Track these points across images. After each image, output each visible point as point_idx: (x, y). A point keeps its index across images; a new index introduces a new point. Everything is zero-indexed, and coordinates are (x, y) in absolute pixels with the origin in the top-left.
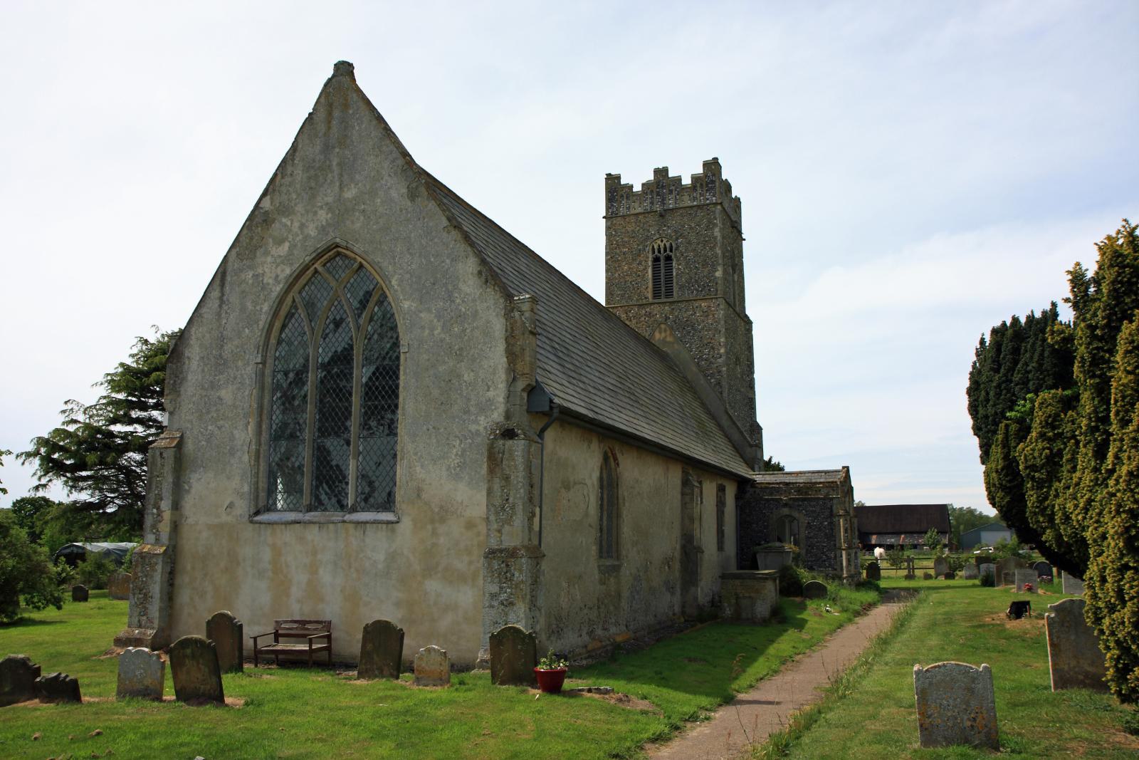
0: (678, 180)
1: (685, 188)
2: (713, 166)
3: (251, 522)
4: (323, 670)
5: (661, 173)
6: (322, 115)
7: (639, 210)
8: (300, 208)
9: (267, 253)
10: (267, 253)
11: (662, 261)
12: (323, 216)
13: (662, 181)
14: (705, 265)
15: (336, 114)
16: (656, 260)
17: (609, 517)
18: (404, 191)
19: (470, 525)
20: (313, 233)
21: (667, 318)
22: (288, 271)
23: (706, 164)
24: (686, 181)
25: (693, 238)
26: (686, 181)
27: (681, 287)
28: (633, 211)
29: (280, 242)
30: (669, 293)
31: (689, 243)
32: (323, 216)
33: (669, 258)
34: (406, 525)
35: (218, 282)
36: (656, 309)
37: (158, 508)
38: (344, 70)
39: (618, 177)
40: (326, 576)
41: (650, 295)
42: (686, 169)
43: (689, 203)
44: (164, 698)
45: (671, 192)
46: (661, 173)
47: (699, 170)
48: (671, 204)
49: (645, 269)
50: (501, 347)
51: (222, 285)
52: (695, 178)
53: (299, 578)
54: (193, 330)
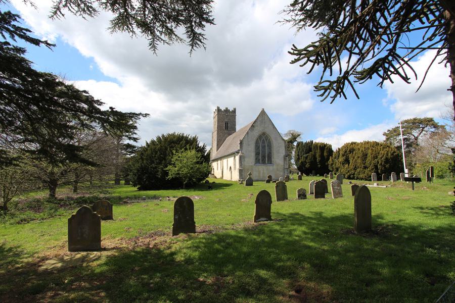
2: (235, 109)
5: (227, 108)
8: (255, 224)
13: (227, 110)
26: (231, 111)
38: (263, 109)
42: (231, 109)
46: (227, 108)
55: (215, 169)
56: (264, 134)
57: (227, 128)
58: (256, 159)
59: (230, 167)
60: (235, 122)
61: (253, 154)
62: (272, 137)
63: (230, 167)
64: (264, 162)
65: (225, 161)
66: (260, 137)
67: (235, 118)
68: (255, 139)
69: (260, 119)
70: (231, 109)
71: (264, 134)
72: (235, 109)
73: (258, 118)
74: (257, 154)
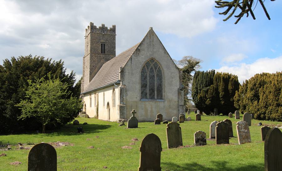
0: (107, 28)
1: (108, 30)
2: (114, 27)
3: (140, 101)
5: (103, 25)
6: (148, 36)
9: (140, 56)
10: (140, 56)
11: (103, 45)
13: (103, 28)
14: (112, 48)
16: (102, 44)
18: (163, 52)
19: (175, 102)
20: (149, 55)
21: (104, 58)
22: (144, 61)
24: (109, 28)
25: (110, 41)
27: (107, 52)
28: (96, 32)
29: (143, 55)
30: (104, 52)
31: (109, 42)
33: (104, 45)
34: (166, 102)
36: (101, 55)
37: (123, 98)
38: (152, 28)
39: (93, 24)
40: (154, 109)
41: (100, 52)
42: (109, 27)
43: (109, 34)
44: (138, 127)
45: (105, 30)
46: (103, 25)
47: (112, 27)
48: (105, 33)
49: (99, 46)
53: (149, 109)
54: (126, 67)
56: (152, 60)
57: (103, 51)
58: (142, 93)
59: (108, 104)
61: (138, 87)
62: (164, 65)
63: (108, 104)
64: (152, 97)
65: (101, 94)
66: (147, 64)
69: (147, 41)
70: (109, 27)
71: (152, 60)
72: (114, 27)
73: (144, 39)
74: (144, 86)
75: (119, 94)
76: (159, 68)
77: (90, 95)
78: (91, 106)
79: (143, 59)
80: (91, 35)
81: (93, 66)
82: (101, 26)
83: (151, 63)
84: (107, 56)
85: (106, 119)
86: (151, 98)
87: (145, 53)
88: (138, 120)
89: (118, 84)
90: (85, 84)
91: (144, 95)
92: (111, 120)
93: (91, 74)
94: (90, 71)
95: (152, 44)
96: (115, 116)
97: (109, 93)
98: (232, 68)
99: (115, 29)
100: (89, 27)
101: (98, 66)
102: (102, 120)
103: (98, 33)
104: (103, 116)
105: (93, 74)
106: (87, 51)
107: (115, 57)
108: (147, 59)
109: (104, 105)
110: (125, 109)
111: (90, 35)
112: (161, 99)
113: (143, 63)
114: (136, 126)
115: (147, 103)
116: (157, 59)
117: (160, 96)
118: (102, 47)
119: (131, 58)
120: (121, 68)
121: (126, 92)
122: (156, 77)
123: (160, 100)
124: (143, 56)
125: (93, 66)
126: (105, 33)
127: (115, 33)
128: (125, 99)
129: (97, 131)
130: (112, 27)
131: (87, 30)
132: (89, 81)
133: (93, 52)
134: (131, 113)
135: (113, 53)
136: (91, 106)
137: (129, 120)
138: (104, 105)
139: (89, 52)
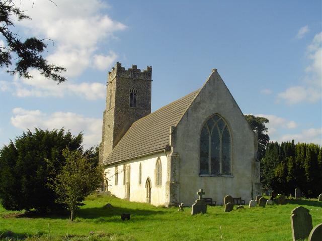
2: (150, 69)
4: (142, 208)
5: (135, 67)
7: (128, 77)
11: (133, 95)
12: (214, 106)
15: (216, 81)
16: (132, 94)
17: (127, 177)
22: (206, 117)
23: (148, 68)
24: (142, 71)
26: (142, 71)
29: (203, 109)
30: (135, 106)
32: (214, 106)
33: (135, 94)
35: (186, 115)
38: (216, 70)
39: (121, 64)
41: (129, 105)
42: (143, 68)
46: (135, 67)
47: (146, 69)
48: (137, 77)
50: (253, 143)
51: (187, 116)
52: (145, 71)
55: (111, 182)
57: (133, 103)
59: (148, 180)
60: (149, 93)
63: (148, 180)
64: (215, 173)
65: (134, 166)
67: (149, 86)
68: (200, 126)
71: (216, 116)
72: (150, 69)
74: (203, 154)
75: (168, 165)
76: (225, 128)
77: (116, 166)
78: (116, 183)
79: (203, 115)
80: (117, 80)
81: (119, 126)
82: (132, 67)
83: (214, 121)
84: (139, 110)
85: (144, 200)
86: (214, 173)
87: (207, 106)
88: (126, 197)
89: (168, 149)
90: (104, 151)
91: (203, 168)
92: (131, 200)
93: (115, 137)
94: (114, 133)
95: (216, 93)
96: (161, 197)
97: (149, 165)
98: (311, 132)
99: (151, 72)
100: (114, 68)
101: (125, 126)
102: (134, 203)
103: (126, 78)
104: (138, 196)
105: (118, 138)
106: (110, 103)
107: (150, 114)
108: (209, 114)
109: (140, 182)
110: (178, 189)
111: (115, 80)
112: (227, 174)
113: (203, 121)
114: (204, 211)
115: (209, 179)
116: (223, 116)
117: (227, 170)
118: (131, 97)
119: (187, 113)
120: (172, 127)
121: (179, 162)
122: (221, 141)
123: (226, 176)
124: (204, 111)
125: (119, 126)
126: (137, 77)
127: (151, 78)
128: (177, 174)
129: (150, 217)
130: (146, 69)
131: (110, 73)
132: (111, 147)
133: (120, 105)
134: (197, 194)
135: (147, 108)
136: (116, 183)
137: (194, 204)
138: (140, 182)
139: (113, 105)
